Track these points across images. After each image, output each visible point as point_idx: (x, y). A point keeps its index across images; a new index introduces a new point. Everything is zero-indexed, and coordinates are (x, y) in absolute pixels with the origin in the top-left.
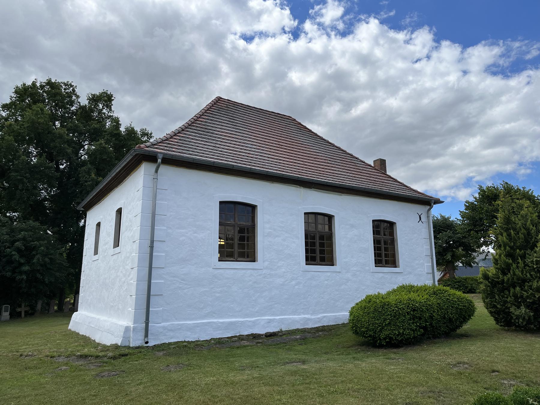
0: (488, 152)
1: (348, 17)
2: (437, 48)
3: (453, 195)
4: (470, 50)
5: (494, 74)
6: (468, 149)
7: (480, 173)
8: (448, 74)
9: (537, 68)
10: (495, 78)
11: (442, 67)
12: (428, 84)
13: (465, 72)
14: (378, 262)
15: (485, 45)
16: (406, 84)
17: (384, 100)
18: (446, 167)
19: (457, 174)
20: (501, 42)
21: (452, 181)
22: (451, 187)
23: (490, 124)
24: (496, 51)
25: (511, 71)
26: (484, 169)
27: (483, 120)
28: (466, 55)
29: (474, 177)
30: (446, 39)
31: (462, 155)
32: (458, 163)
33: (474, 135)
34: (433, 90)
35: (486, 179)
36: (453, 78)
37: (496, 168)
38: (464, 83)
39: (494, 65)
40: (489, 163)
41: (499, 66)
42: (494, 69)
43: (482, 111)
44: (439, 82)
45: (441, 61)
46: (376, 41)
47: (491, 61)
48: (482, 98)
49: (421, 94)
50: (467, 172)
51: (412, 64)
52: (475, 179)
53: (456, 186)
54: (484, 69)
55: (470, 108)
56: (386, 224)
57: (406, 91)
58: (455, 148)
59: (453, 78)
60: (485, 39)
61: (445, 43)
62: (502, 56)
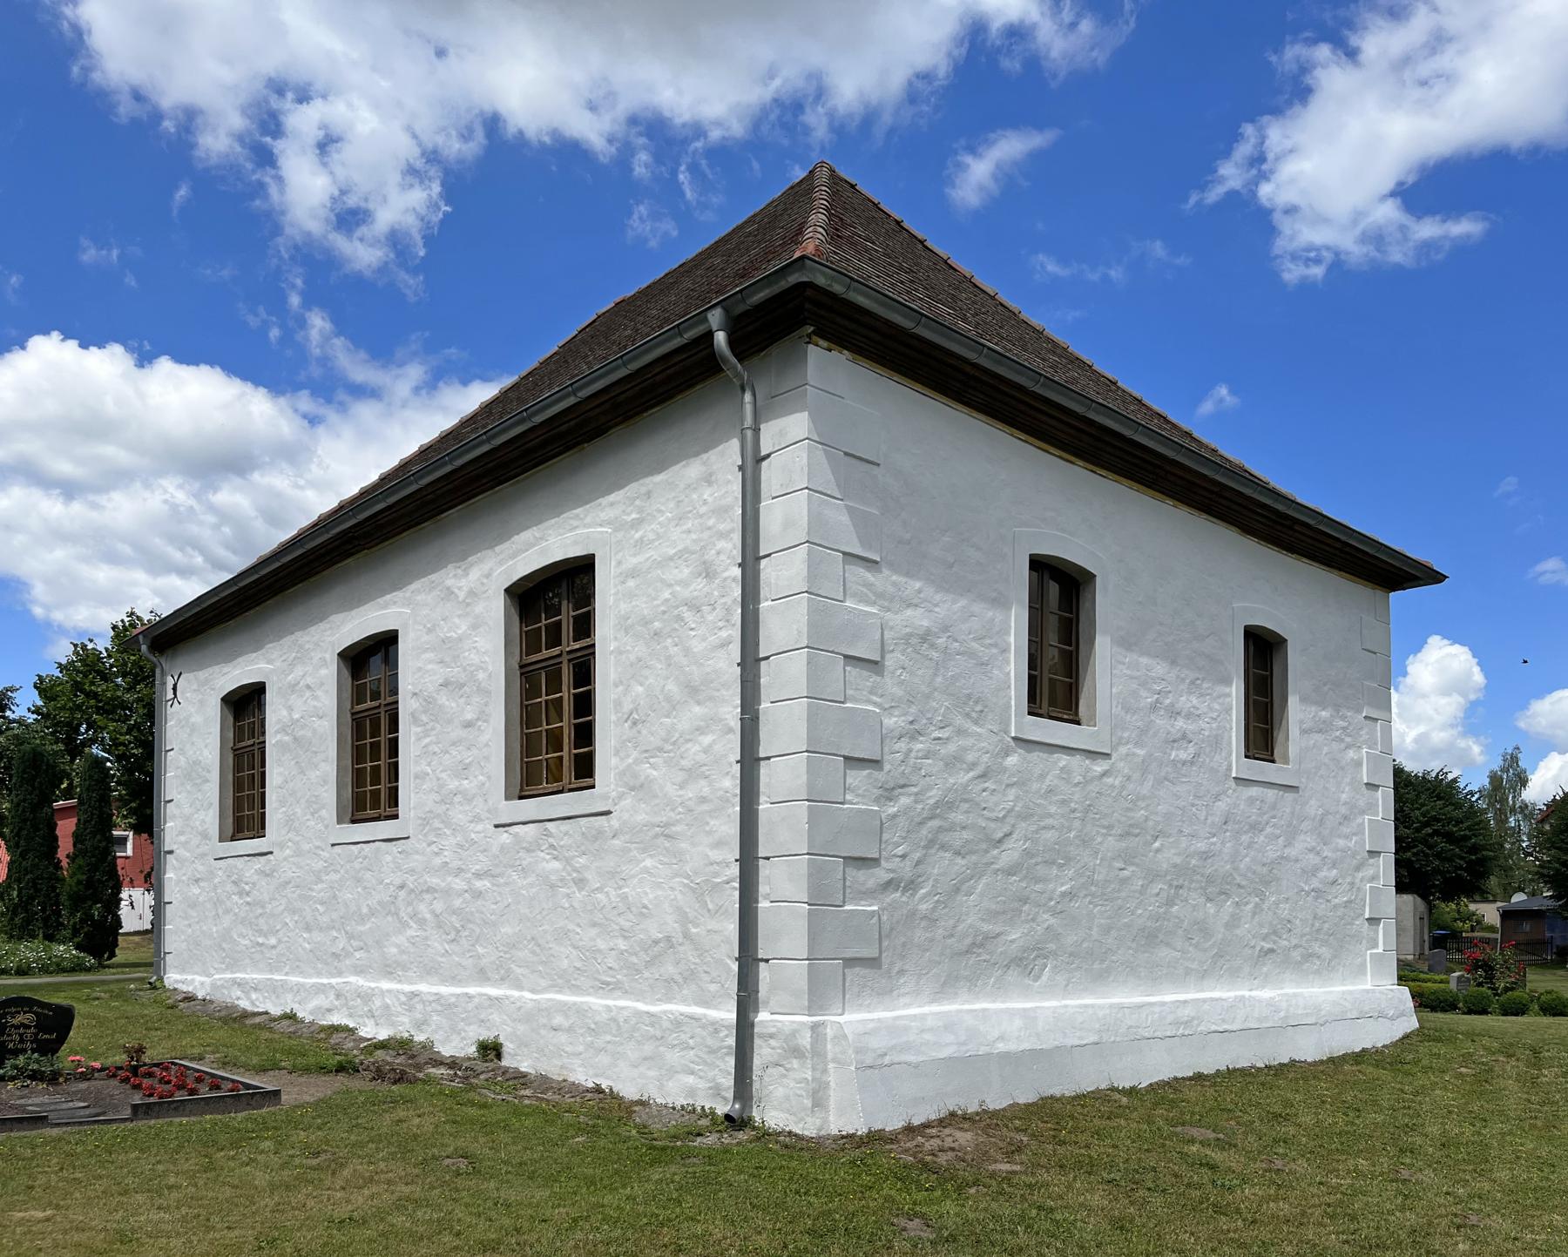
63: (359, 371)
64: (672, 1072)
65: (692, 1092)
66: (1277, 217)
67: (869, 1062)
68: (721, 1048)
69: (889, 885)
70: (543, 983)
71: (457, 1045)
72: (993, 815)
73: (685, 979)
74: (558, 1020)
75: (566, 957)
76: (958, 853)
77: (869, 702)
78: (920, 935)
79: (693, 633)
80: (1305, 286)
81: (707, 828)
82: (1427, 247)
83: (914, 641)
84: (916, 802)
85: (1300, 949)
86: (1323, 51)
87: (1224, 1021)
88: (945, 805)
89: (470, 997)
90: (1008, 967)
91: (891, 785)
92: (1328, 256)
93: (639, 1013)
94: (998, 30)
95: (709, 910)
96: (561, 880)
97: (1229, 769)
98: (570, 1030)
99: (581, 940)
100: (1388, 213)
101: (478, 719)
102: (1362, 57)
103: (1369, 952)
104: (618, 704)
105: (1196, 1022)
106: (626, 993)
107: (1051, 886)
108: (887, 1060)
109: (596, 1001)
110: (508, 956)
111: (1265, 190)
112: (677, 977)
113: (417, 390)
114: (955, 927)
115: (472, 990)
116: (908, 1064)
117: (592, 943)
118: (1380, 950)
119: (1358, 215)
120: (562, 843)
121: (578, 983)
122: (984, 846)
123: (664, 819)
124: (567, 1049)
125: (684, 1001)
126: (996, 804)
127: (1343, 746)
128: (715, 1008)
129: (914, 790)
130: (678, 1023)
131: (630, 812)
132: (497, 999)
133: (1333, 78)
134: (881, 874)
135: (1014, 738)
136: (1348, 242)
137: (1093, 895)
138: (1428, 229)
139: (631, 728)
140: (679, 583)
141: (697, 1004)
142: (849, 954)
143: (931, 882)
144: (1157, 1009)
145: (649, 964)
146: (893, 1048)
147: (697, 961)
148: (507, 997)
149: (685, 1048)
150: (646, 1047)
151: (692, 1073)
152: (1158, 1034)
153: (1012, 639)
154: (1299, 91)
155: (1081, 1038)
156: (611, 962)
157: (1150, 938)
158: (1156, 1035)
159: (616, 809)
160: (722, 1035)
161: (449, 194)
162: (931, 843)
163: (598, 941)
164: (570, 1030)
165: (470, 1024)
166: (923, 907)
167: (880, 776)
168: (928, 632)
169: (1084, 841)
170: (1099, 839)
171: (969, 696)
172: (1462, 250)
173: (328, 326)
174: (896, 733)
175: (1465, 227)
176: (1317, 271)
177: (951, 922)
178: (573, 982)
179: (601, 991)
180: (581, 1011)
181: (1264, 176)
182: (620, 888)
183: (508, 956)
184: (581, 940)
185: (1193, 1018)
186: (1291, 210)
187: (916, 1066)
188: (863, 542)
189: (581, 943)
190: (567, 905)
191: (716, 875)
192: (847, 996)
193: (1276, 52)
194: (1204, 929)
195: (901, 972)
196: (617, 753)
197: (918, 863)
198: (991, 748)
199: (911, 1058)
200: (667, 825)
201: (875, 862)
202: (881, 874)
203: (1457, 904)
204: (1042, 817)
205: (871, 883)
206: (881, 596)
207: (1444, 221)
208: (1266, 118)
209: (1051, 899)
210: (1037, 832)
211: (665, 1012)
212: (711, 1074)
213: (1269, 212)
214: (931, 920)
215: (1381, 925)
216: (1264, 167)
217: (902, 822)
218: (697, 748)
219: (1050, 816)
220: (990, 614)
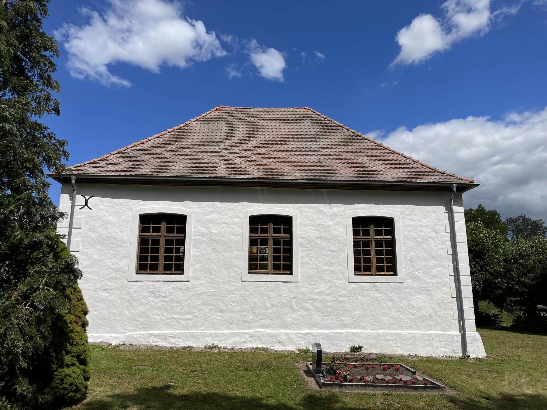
64: (437, 348)
65: (445, 352)
66: (70, 55)
68: (454, 341)
70: (377, 328)
71: (345, 348)
73: (436, 325)
74: (388, 338)
75: (386, 320)
79: (432, 244)
80: (77, 80)
81: (441, 290)
82: (113, 84)
86: (96, 14)
89: (342, 333)
92: (85, 74)
93: (421, 334)
95: (443, 308)
96: (383, 299)
98: (393, 340)
99: (393, 315)
100: (103, 69)
101: (339, 250)
102: (108, 23)
104: (405, 256)
106: (414, 329)
109: (405, 332)
110: (359, 320)
111: (66, 45)
112: (434, 325)
115: (342, 331)
117: (399, 316)
119: (96, 67)
120: (383, 289)
121: (393, 327)
123: (425, 286)
124: (393, 345)
125: (436, 330)
128: (448, 331)
130: (437, 336)
131: (409, 282)
132: (357, 333)
133: (98, 24)
136: (91, 72)
138: (115, 79)
139: (410, 263)
140: (427, 232)
141: (441, 331)
145: (422, 322)
147: (440, 320)
148: (361, 332)
149: (440, 342)
150: (427, 342)
151: (444, 348)
154: (87, 21)
156: (407, 321)
159: (405, 283)
160: (454, 338)
163: (401, 315)
164: (393, 340)
165: (342, 342)
172: (123, 87)
175: (126, 83)
176: (81, 77)
178: (391, 327)
179: (403, 329)
180: (399, 335)
181: (68, 42)
182: (409, 302)
183: (359, 320)
184: (393, 315)
186: (75, 55)
189: (393, 316)
190: (386, 306)
191: (445, 300)
193: (80, 7)
196: (405, 268)
200: (426, 288)
207: (120, 79)
208: (71, 25)
211: (433, 333)
212: (451, 347)
213: (68, 53)
216: (68, 39)
218: (435, 270)
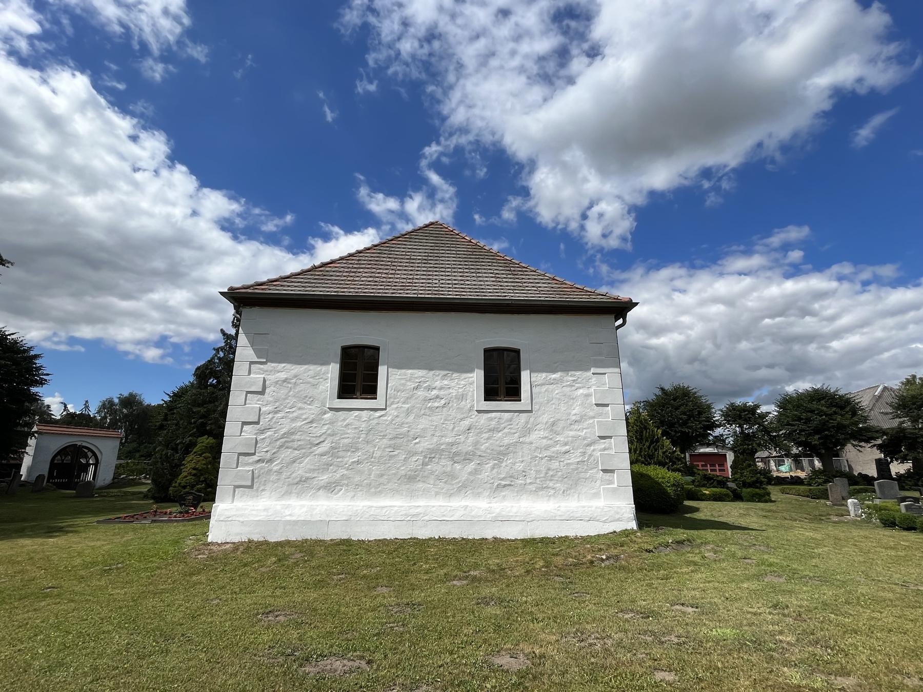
0: (193, 313)
1: (45, 45)
2: (171, 167)
3: (137, 352)
4: (206, 191)
5: (223, 229)
6: (172, 303)
7: (179, 334)
8: (174, 204)
9: (917, 285)
10: (222, 233)
11: (171, 195)
12: (145, 205)
13: (195, 213)
14: (491, 394)
15: (224, 196)
16: (111, 188)
17: (72, 194)
18: (136, 316)
19: (149, 327)
20: (243, 200)
21: (139, 335)
22: (138, 343)
23: (203, 281)
24: (235, 207)
25: (243, 233)
26: (184, 330)
27: (195, 274)
28: (200, 195)
29: (171, 337)
30: (183, 163)
31: (162, 307)
32: (155, 314)
33: (180, 287)
34: (150, 215)
35: (185, 343)
36: (179, 212)
37: (197, 332)
38: (189, 224)
39: (227, 220)
40: (192, 324)
41: (233, 223)
42: (226, 225)
43: (198, 263)
44: (160, 209)
45: (171, 185)
46: (83, 106)
47: (227, 215)
48: (201, 248)
49: (131, 211)
50: (160, 329)
51: (133, 172)
52: (172, 340)
53: (145, 343)
54: (216, 219)
55: (186, 254)
56: (513, 353)
57: (102, 197)
58: (156, 296)
59: (179, 212)
60: (227, 188)
61: (181, 168)
62: (239, 215)
63: (624, 276)
67: (222, 519)
69: (258, 461)
72: (314, 435)
76: (296, 449)
77: (256, 404)
78: (273, 477)
83: (280, 382)
84: (275, 433)
85: (536, 485)
87: (444, 516)
88: (290, 433)
90: (319, 489)
91: (263, 429)
94: (231, 198)
97: (473, 406)
103: (602, 487)
105: (422, 515)
107: (346, 459)
108: (230, 519)
113: (642, 276)
114: (291, 475)
116: (239, 521)
118: (615, 486)
122: (309, 446)
126: (316, 432)
127: (573, 388)
129: (274, 429)
134: (255, 458)
135: (328, 408)
137: (373, 462)
142: (237, 484)
143: (280, 459)
144: (396, 508)
146: (235, 515)
152: (391, 519)
153: (330, 375)
155: (337, 518)
157: (411, 478)
158: (389, 519)
161: (637, 219)
162: (281, 447)
166: (275, 468)
167: (258, 426)
168: (286, 379)
169: (367, 442)
170: (377, 441)
171: (306, 397)
173: (608, 268)
174: (268, 412)
177: (289, 474)
185: (421, 513)
187: (243, 522)
188: (258, 357)
192: (236, 493)
194: (452, 476)
195: (263, 490)
197: (274, 453)
198: (315, 413)
199: (241, 519)
201: (254, 454)
202: (255, 458)
203: (639, 470)
204: (342, 434)
205: (251, 461)
206: (267, 371)
209: (346, 464)
210: (339, 440)
214: (279, 472)
215: (615, 475)
217: (268, 441)
219: (348, 433)
220: (319, 369)
